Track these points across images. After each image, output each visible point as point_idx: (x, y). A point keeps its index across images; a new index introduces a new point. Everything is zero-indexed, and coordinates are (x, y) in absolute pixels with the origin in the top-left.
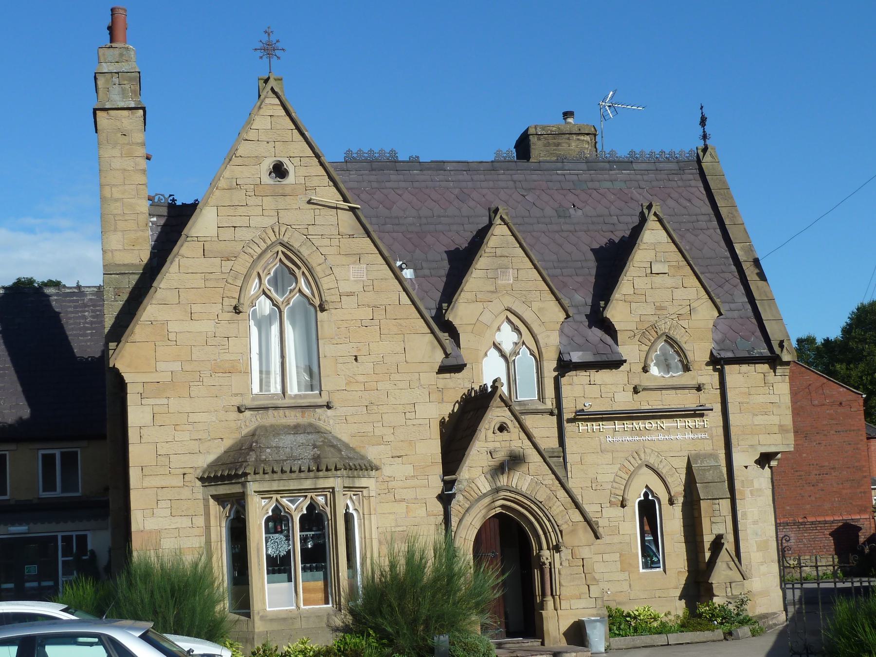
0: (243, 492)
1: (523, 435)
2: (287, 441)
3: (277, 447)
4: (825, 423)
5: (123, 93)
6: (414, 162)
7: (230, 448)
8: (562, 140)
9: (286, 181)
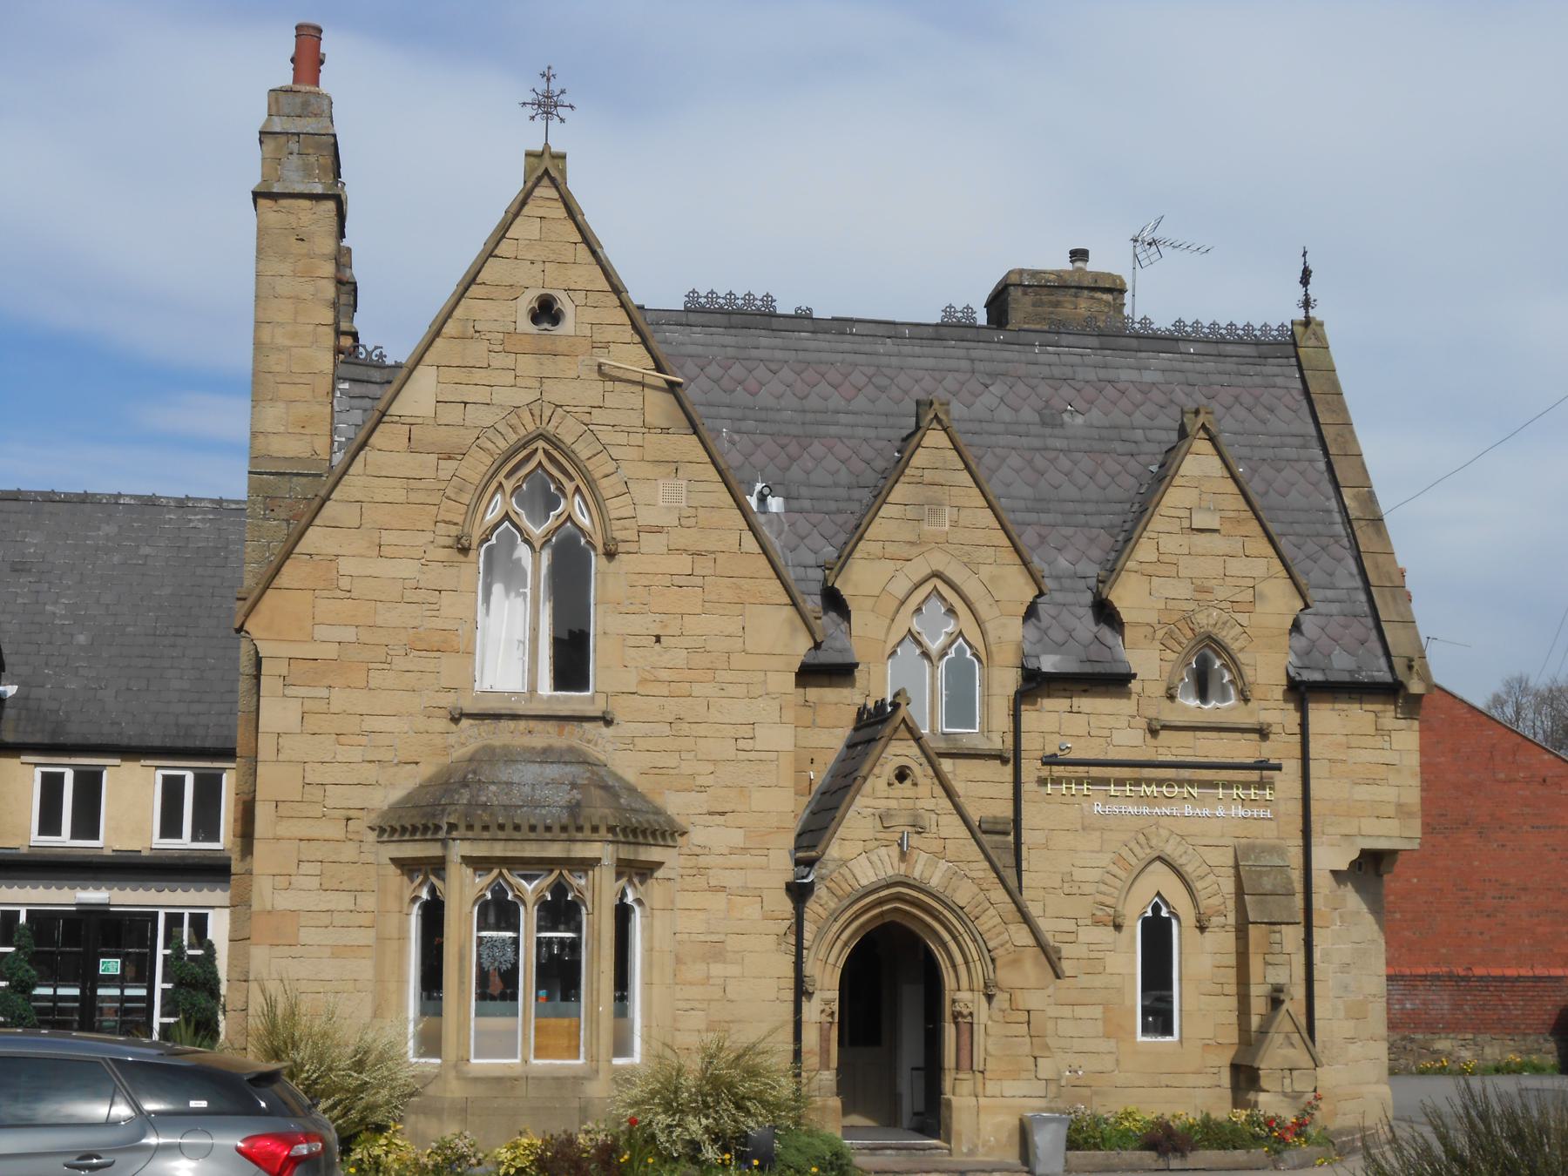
0: (444, 858)
1: (939, 791)
2: (528, 773)
3: (509, 784)
4: (1515, 811)
5: (307, 171)
6: (803, 318)
7: (430, 780)
8: (1066, 298)
9: (560, 330)
